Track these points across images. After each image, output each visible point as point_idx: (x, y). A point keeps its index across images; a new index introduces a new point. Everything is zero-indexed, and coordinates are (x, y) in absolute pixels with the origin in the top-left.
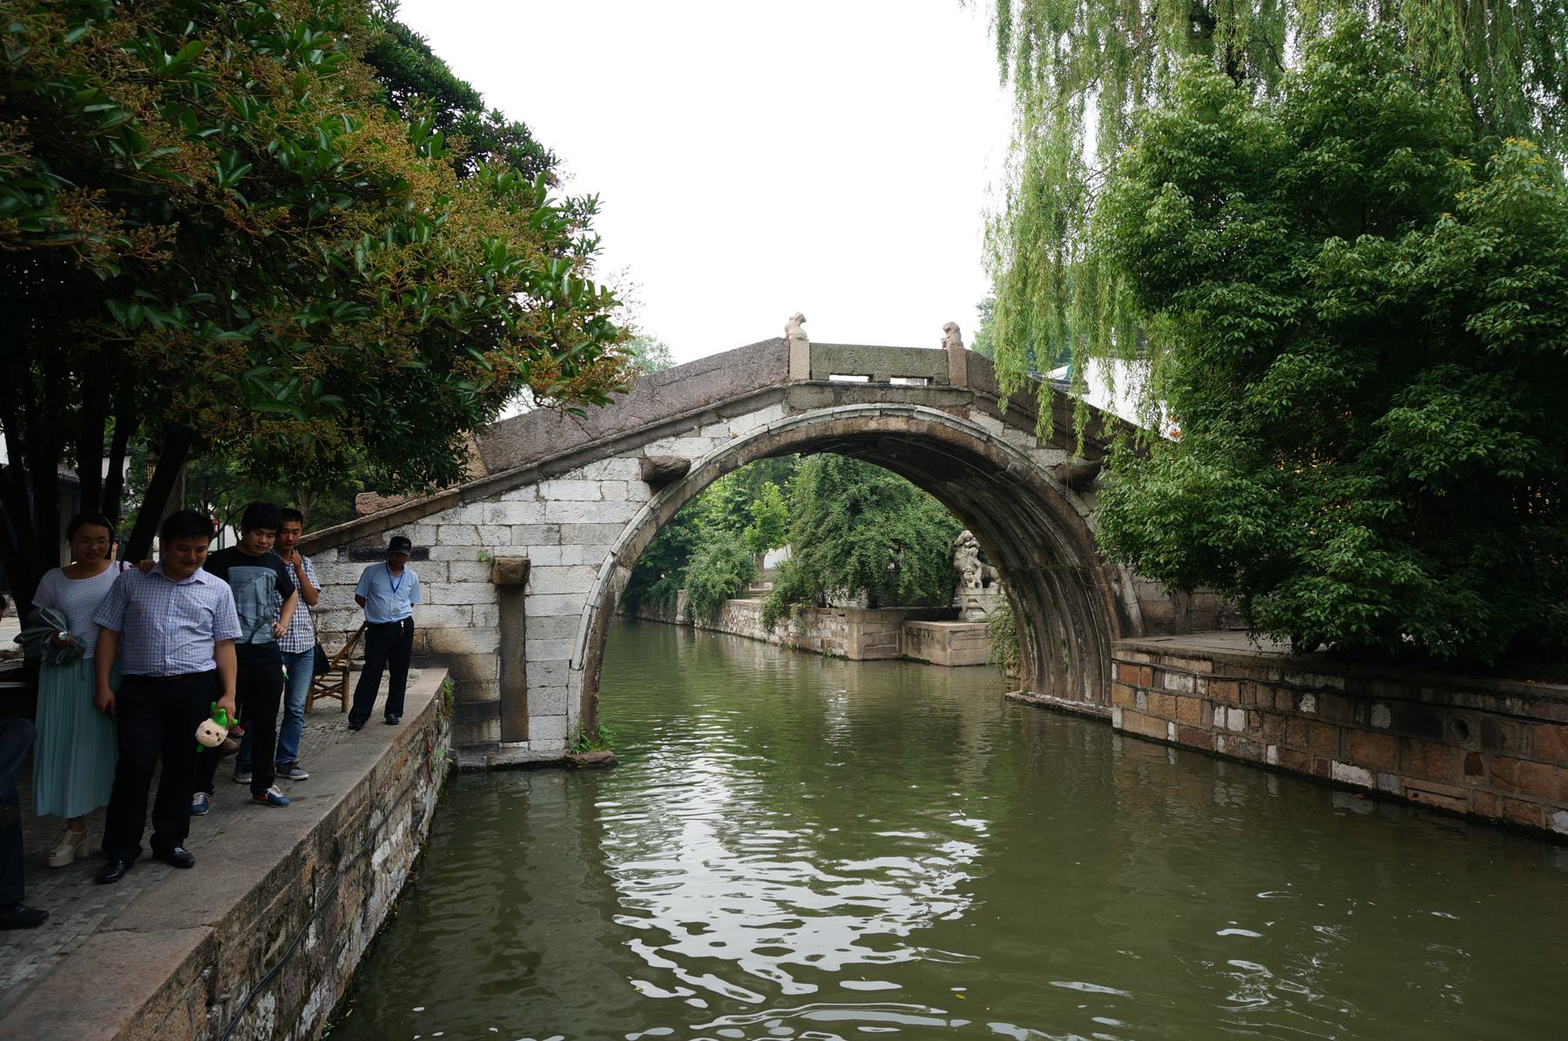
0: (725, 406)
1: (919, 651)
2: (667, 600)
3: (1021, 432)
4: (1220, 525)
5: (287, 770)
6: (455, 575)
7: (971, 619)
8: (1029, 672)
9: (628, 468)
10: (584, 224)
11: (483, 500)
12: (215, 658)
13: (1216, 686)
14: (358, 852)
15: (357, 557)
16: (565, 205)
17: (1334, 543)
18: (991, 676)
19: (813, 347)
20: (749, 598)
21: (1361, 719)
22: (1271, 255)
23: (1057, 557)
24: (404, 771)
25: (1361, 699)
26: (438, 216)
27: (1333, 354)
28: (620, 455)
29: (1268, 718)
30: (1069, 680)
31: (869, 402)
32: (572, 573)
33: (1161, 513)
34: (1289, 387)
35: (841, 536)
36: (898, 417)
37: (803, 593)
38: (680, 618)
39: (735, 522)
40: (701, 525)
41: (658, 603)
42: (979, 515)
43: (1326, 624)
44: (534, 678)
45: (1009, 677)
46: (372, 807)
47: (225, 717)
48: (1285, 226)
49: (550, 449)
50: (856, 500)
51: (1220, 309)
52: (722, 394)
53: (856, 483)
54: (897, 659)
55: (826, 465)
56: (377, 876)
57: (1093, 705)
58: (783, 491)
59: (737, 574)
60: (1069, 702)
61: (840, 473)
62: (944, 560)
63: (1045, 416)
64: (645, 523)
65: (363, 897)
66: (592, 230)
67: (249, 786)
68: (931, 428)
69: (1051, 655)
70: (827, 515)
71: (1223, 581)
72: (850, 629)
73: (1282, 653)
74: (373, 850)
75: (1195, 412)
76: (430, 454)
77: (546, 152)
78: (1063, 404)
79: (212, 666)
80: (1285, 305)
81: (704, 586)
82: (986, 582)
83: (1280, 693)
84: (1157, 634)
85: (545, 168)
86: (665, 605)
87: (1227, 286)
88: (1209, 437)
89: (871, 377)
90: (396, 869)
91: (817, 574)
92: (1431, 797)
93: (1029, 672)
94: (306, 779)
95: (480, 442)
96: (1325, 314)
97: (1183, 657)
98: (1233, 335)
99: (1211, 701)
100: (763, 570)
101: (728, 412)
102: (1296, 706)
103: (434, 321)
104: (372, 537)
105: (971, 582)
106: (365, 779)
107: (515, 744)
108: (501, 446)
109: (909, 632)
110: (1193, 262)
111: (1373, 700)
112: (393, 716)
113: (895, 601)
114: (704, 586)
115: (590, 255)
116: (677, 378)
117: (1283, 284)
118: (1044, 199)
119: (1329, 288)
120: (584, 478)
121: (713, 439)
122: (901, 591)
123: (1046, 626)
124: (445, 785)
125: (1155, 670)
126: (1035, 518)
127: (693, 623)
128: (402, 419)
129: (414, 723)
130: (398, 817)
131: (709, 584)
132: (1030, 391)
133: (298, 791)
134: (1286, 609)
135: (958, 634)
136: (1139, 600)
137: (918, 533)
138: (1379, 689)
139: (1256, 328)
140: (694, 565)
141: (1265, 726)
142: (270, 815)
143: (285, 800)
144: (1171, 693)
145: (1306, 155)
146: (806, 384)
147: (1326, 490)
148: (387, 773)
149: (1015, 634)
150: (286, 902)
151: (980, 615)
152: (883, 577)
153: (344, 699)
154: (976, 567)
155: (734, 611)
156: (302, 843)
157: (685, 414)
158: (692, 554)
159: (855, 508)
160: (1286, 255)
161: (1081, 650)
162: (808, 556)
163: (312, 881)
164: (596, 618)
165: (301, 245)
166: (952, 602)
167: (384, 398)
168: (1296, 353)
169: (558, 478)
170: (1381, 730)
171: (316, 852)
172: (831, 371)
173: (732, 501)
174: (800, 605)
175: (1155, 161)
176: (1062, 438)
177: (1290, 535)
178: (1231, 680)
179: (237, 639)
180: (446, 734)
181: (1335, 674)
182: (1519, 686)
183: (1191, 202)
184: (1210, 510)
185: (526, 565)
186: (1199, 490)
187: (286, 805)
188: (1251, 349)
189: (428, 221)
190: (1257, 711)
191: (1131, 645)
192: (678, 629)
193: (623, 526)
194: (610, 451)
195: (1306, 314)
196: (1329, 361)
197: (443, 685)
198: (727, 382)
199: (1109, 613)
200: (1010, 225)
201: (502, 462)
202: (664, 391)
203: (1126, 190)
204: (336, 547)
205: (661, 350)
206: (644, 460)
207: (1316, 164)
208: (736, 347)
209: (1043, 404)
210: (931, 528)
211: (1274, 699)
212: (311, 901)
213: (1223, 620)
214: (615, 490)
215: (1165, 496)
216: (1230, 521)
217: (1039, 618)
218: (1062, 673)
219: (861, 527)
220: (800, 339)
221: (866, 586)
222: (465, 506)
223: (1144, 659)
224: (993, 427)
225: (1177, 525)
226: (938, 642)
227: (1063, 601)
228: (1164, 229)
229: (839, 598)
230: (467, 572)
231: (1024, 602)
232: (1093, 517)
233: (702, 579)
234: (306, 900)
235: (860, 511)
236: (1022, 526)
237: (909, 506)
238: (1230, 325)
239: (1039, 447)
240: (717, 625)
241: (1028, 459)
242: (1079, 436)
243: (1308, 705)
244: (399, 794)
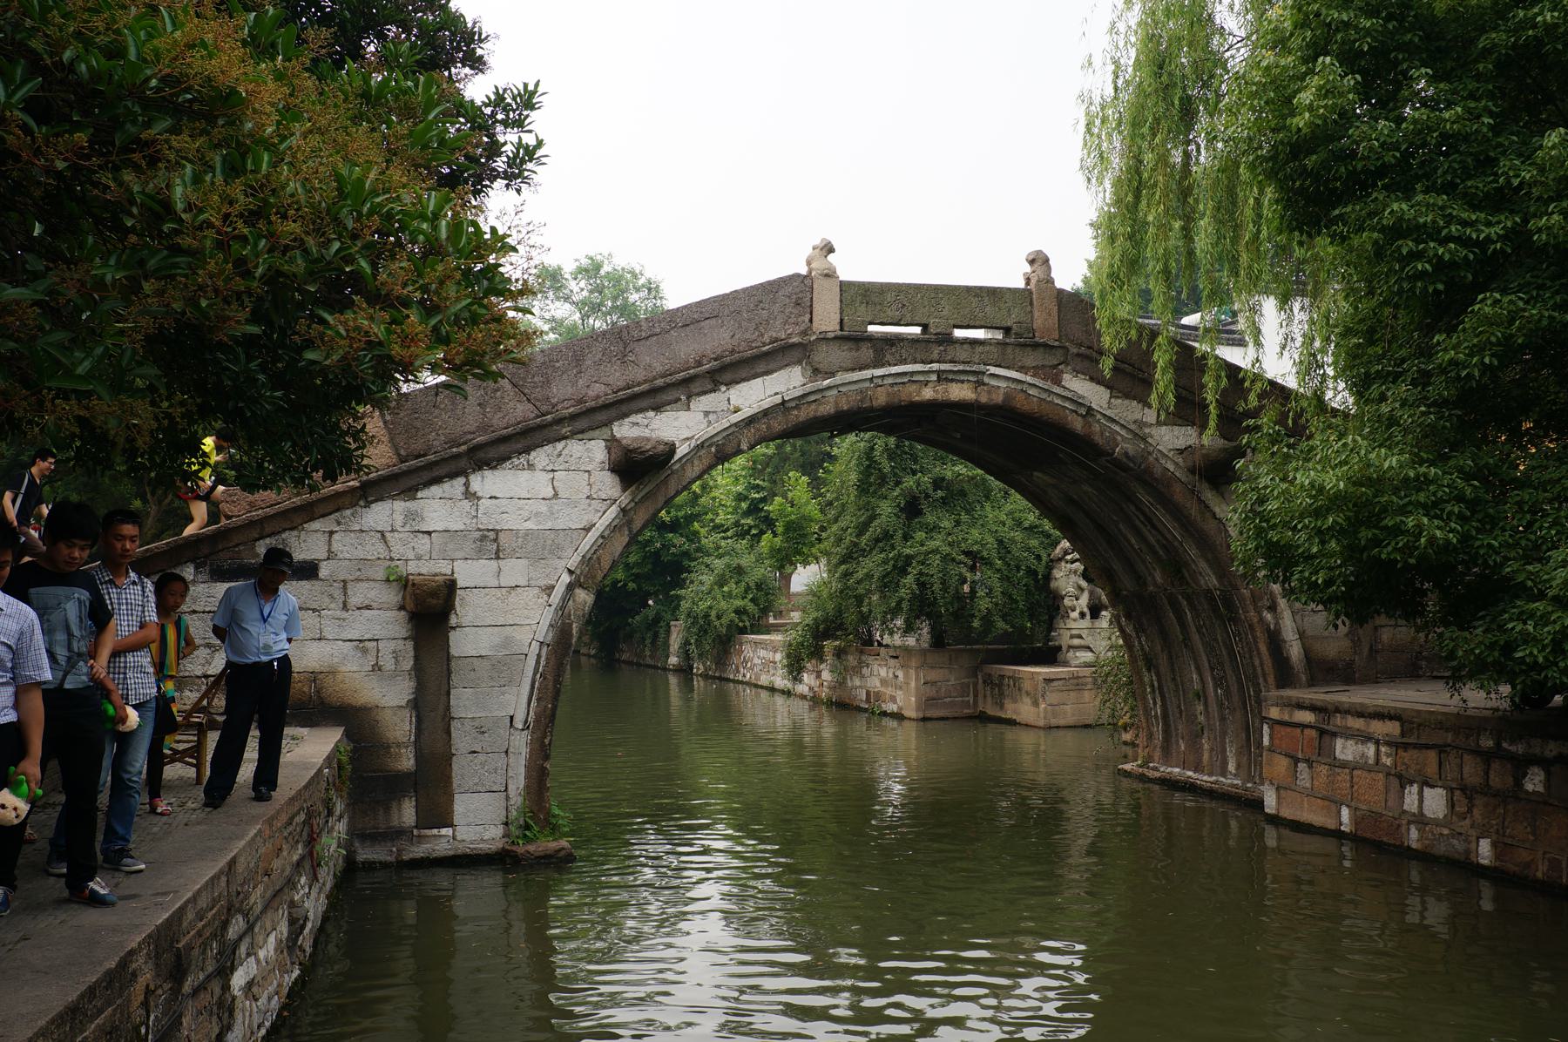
0: (723, 368)
1: (1002, 706)
2: (656, 635)
3: (1134, 403)
4: (1397, 530)
5: (116, 859)
6: (354, 600)
7: (1074, 663)
8: (1150, 736)
9: (592, 452)
10: (519, 124)
11: (393, 498)
12: (16, 706)
13: (1406, 756)
14: (210, 969)
15: (219, 575)
16: (493, 97)
18: (1098, 744)
19: (845, 287)
20: (768, 633)
22: (1471, 154)
23: (1186, 574)
24: (276, 864)
26: (284, 138)
27: (1557, 293)
28: (580, 436)
29: (1480, 801)
30: (1206, 746)
31: (923, 362)
32: (513, 598)
33: (1318, 513)
34: (1493, 339)
35: (893, 547)
36: (962, 382)
37: (841, 627)
38: (673, 660)
39: (751, 527)
40: (703, 531)
41: (644, 639)
43: (1547, 668)
44: (461, 740)
45: (1125, 743)
46: (230, 910)
47: (25, 785)
48: (1491, 114)
49: (483, 428)
50: (915, 498)
51: (1398, 230)
52: (719, 351)
53: (914, 473)
54: (970, 718)
55: (872, 449)
56: (238, 1004)
57: (1239, 782)
58: (816, 484)
59: (752, 600)
60: (1205, 778)
61: (891, 459)
62: (1036, 581)
63: (1163, 380)
64: (614, 528)
65: (216, 1030)
66: (530, 131)
67: (63, 880)
68: (1007, 396)
69: (1181, 712)
70: (873, 518)
71: (1410, 609)
72: (906, 676)
73: (1497, 710)
74: (233, 969)
75: (1367, 374)
76: (312, 435)
77: (469, 25)
78: (1188, 363)
79: (11, 717)
80: (1489, 224)
81: (707, 616)
82: (1095, 611)
83: (1496, 765)
84: (1327, 682)
85: (468, 47)
86: (653, 642)
87: (1408, 199)
88: (1385, 409)
89: (925, 327)
90: (265, 995)
91: (859, 600)
93: (1150, 736)
94: (141, 871)
95: (388, 418)
96: (1544, 237)
97: (1360, 715)
98: (1415, 267)
99: (1400, 777)
100: (789, 595)
101: (728, 376)
102: (1518, 783)
103: (274, 277)
104: (241, 548)
105: (1073, 610)
106: (221, 872)
107: (435, 831)
108: (418, 424)
109: (988, 681)
110: (1359, 166)
112: (263, 789)
114: (707, 616)
115: (530, 166)
116: (658, 330)
117: (1487, 195)
118: (1165, 78)
119: (1551, 199)
120: (531, 467)
121: (707, 414)
122: (976, 624)
123: (1173, 671)
124: (337, 887)
125: (1322, 732)
126: (1155, 521)
127: (691, 668)
128: (273, 389)
129: (292, 799)
130: (268, 925)
131: (713, 613)
132: (1144, 346)
133: (129, 885)
134: (1492, 646)
135: (1056, 683)
136: (1302, 635)
137: (1000, 542)
139: (1447, 257)
140: (693, 587)
141: (1475, 811)
142: (91, 917)
143: (109, 898)
144: (1344, 765)
145: (1521, 13)
146: (836, 338)
147: (1550, 481)
148: (252, 865)
149: (1131, 682)
150: (108, 1029)
151: (1087, 656)
152: (952, 603)
153: (199, 767)
154: (1081, 589)
155: (748, 651)
156: (131, 953)
157: (668, 380)
158: (690, 572)
159: (911, 508)
160: (1492, 154)
161: (1221, 705)
162: (846, 575)
163: (145, 1005)
164: (547, 659)
165: (104, 180)
166: (1048, 639)
167: (250, 359)
168: (1504, 292)
169: (495, 468)
171: (150, 965)
172: (869, 319)
173: (746, 498)
174: (837, 643)
175: (1309, 26)
176: (1188, 409)
177: (1496, 544)
178: (1427, 747)
179: (45, 683)
180: (341, 817)
183: (1357, 83)
184: (1384, 510)
185: (451, 586)
186: (1368, 482)
187: (113, 904)
188: (1440, 287)
189: (270, 147)
190: (1463, 789)
191: (1289, 698)
193: (583, 532)
194: (565, 430)
195: (1518, 236)
196: (1551, 302)
197: (336, 749)
198: (727, 335)
199: (1259, 654)
200: (1117, 115)
201: (418, 446)
202: (640, 348)
203: (1268, 68)
204: (192, 561)
205: (650, 290)
206: (612, 442)
207: (1535, 26)
208: (739, 287)
209: (1161, 364)
210: (1018, 535)
211: (1487, 773)
212: (143, 1031)
213: (1424, 663)
214: (573, 485)
215: (1321, 489)
216: (1411, 524)
217: (1163, 661)
219: (920, 535)
220: (827, 275)
221: (929, 616)
222: (368, 505)
223: (1307, 717)
224: (1094, 395)
225: (1337, 531)
226: (1028, 694)
227: (1196, 637)
228: (1319, 122)
229: (891, 633)
230: (372, 594)
231: (1143, 639)
232: (1231, 514)
233: (703, 606)
234: (137, 1029)
235: (919, 513)
236: (1138, 533)
237: (987, 505)
238: (1410, 253)
239: (1159, 423)
240: (725, 671)
241: (1144, 439)
242: (1211, 407)
243: (1534, 782)
244: (269, 894)
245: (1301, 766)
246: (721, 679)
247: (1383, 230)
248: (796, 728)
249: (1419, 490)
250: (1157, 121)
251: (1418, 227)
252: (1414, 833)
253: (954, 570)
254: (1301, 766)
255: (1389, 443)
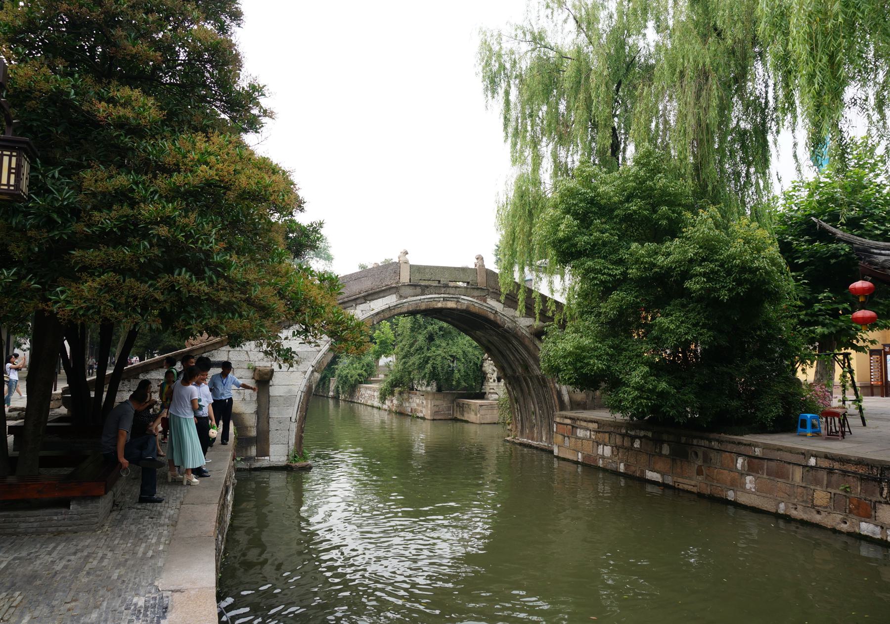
0: (369, 295)
1: (463, 415)
2: (324, 383)
4: (588, 364)
8: (516, 427)
13: (599, 435)
17: (634, 373)
18: (498, 430)
20: (371, 383)
21: (657, 450)
25: (658, 441)
29: (621, 450)
33: (565, 357)
35: (423, 353)
38: (331, 394)
42: (492, 348)
44: (273, 425)
50: (432, 334)
53: (432, 324)
54: (451, 419)
62: (477, 367)
68: (468, 307)
70: (416, 341)
72: (427, 403)
80: (616, 269)
81: (346, 376)
83: (626, 439)
84: (577, 409)
88: (587, 323)
91: (410, 373)
92: (684, 486)
93: (516, 427)
97: (585, 421)
99: (597, 442)
101: (370, 298)
102: (632, 445)
109: (458, 405)
111: (663, 442)
113: (451, 387)
114: (346, 376)
121: (362, 311)
122: (454, 383)
125: (573, 427)
131: (349, 375)
134: (616, 401)
137: (464, 352)
138: (665, 437)
144: (579, 438)
151: (496, 396)
155: (363, 391)
157: (349, 299)
159: (431, 338)
161: (541, 416)
162: (405, 363)
166: (481, 389)
168: (621, 290)
170: (665, 456)
178: (605, 432)
181: (648, 430)
182: (716, 436)
185: (272, 371)
192: (330, 400)
195: (624, 274)
198: (370, 283)
210: (470, 349)
217: (521, 400)
218: (532, 427)
219: (433, 349)
221: (436, 380)
223: (568, 421)
224: (498, 306)
230: (242, 373)
233: (345, 372)
236: (513, 354)
237: (459, 338)
243: (637, 444)
245: (566, 438)
246: (351, 402)
247: (585, 270)
248: (383, 422)
249: (595, 351)
250: (520, 216)
251: (596, 269)
252: (601, 462)
253: (446, 362)
254: (566, 438)
255: (587, 336)
